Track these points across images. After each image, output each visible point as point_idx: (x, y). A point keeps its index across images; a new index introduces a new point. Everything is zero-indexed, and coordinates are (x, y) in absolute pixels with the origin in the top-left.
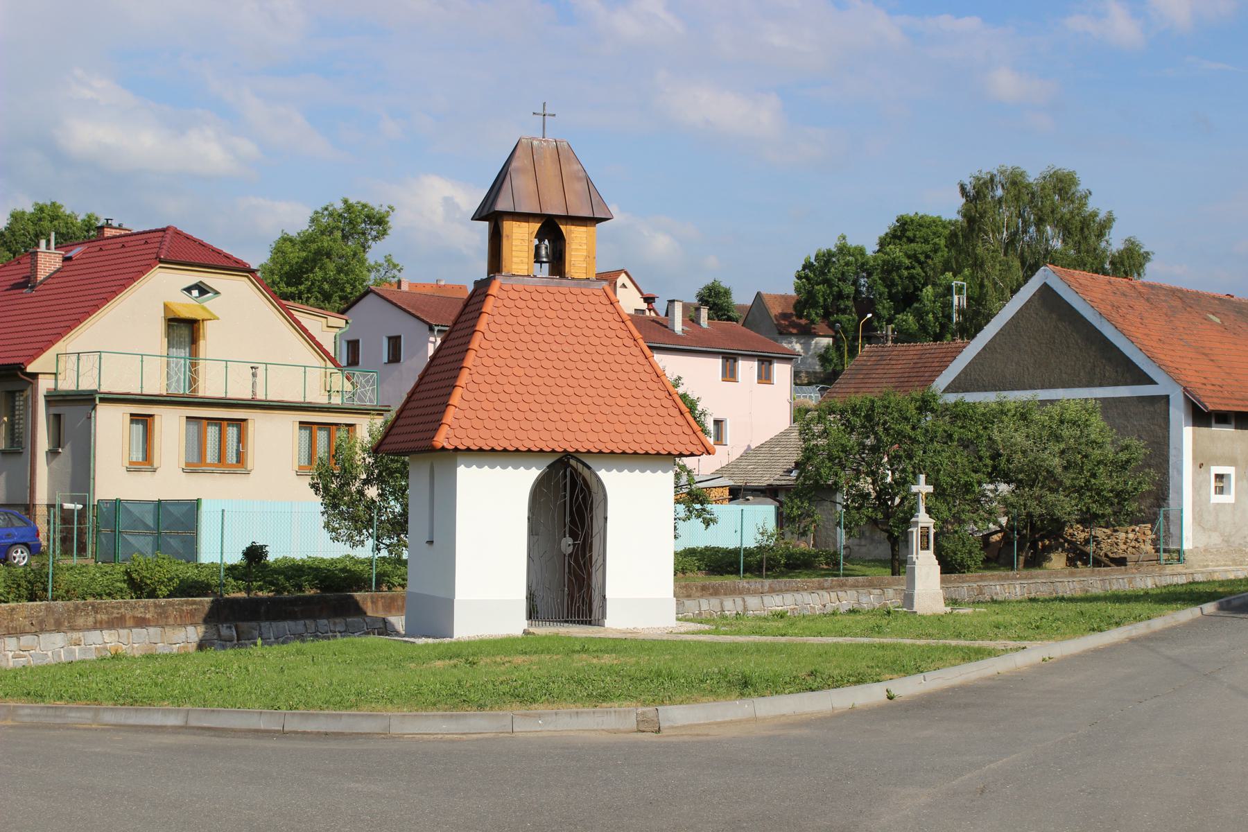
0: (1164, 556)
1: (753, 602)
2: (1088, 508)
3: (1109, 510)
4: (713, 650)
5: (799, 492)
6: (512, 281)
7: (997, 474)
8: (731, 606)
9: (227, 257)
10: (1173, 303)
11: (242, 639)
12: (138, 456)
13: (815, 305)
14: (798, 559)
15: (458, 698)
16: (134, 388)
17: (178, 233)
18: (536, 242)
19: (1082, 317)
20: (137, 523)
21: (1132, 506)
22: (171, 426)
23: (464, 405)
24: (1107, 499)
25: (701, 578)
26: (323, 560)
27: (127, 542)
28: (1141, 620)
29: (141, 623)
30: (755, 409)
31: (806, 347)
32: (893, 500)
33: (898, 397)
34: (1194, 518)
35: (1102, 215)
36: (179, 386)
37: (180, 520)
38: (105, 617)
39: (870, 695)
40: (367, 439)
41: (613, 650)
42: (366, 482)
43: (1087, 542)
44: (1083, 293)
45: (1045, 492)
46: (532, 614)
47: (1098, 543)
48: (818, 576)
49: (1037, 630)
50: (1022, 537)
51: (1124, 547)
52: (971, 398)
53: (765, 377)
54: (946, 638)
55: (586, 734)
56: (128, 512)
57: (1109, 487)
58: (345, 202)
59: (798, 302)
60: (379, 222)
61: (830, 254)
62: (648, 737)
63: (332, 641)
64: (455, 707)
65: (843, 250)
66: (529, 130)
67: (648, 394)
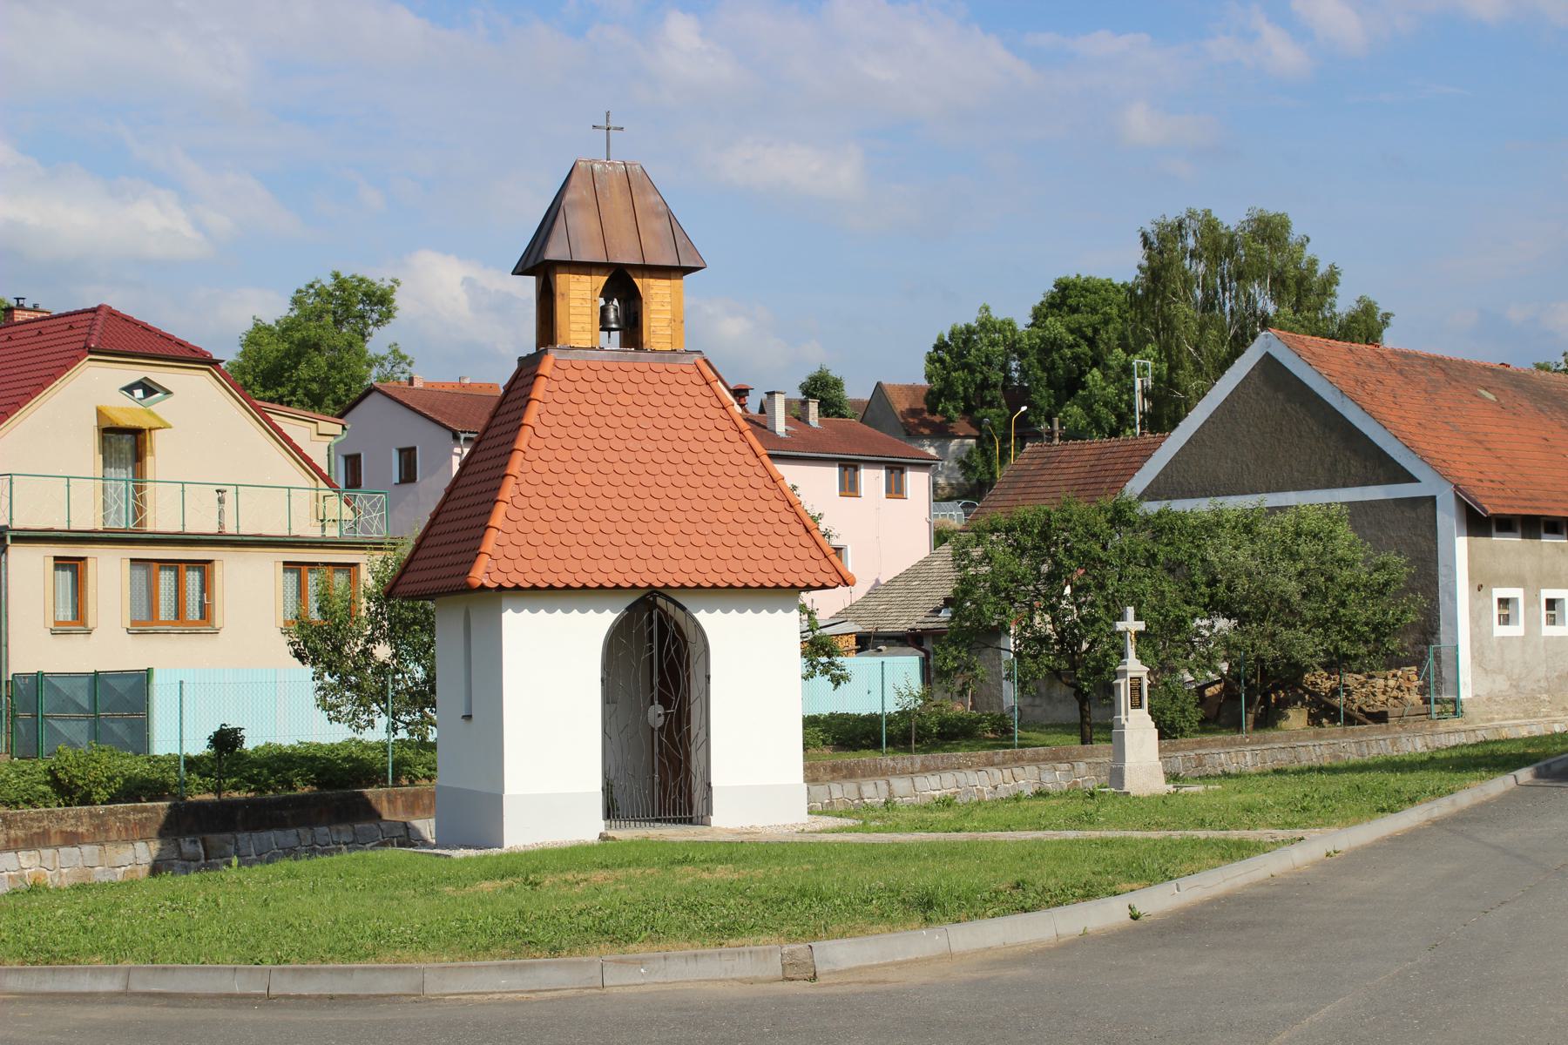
0: (1435, 708)
1: (901, 785)
2: (1336, 648)
3: (1363, 650)
4: (870, 855)
5: (950, 641)
6: (572, 355)
7: (1216, 606)
8: (874, 792)
9: (180, 344)
10: (1434, 376)
11: (211, 860)
12: (66, 613)
13: (952, 397)
14: (955, 726)
15: (521, 939)
16: (58, 523)
17: (113, 314)
18: (602, 302)
19: (1317, 397)
20: (67, 704)
21: (1394, 644)
22: (109, 571)
23: (510, 527)
24: (1361, 636)
25: (828, 755)
26: (320, 746)
27: (55, 733)
28: (1441, 795)
29: (72, 839)
30: (888, 530)
31: (942, 450)
32: (1079, 644)
33: (1080, 507)
34: (1473, 657)
35: (1322, 269)
36: (120, 518)
37: (123, 699)
38: (20, 833)
39: (1106, 914)
40: (371, 582)
41: (729, 859)
42: (371, 640)
43: (1334, 692)
44: (1318, 367)
45: (1279, 629)
46: (611, 812)
47: (1349, 693)
48: (983, 748)
49: (1304, 813)
50: (1251, 690)
51: (1383, 698)
52: (1179, 506)
53: (895, 490)
54: (1185, 828)
55: (710, 986)
56: (57, 690)
57: (1363, 618)
58: (336, 276)
59: (930, 392)
60: (380, 300)
61: (969, 330)
62: (800, 988)
63: (336, 857)
64: (517, 952)
65: (986, 326)
66: (589, 149)
67: (762, 505)
